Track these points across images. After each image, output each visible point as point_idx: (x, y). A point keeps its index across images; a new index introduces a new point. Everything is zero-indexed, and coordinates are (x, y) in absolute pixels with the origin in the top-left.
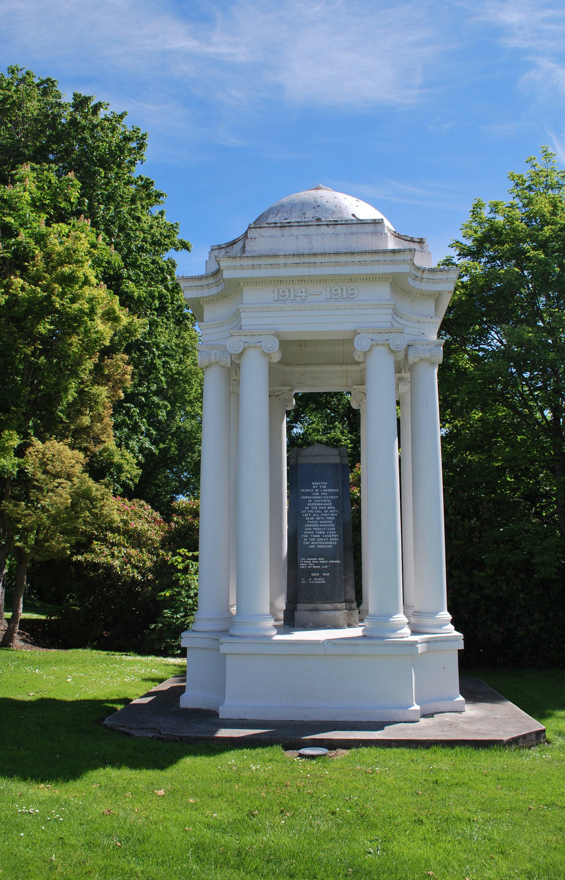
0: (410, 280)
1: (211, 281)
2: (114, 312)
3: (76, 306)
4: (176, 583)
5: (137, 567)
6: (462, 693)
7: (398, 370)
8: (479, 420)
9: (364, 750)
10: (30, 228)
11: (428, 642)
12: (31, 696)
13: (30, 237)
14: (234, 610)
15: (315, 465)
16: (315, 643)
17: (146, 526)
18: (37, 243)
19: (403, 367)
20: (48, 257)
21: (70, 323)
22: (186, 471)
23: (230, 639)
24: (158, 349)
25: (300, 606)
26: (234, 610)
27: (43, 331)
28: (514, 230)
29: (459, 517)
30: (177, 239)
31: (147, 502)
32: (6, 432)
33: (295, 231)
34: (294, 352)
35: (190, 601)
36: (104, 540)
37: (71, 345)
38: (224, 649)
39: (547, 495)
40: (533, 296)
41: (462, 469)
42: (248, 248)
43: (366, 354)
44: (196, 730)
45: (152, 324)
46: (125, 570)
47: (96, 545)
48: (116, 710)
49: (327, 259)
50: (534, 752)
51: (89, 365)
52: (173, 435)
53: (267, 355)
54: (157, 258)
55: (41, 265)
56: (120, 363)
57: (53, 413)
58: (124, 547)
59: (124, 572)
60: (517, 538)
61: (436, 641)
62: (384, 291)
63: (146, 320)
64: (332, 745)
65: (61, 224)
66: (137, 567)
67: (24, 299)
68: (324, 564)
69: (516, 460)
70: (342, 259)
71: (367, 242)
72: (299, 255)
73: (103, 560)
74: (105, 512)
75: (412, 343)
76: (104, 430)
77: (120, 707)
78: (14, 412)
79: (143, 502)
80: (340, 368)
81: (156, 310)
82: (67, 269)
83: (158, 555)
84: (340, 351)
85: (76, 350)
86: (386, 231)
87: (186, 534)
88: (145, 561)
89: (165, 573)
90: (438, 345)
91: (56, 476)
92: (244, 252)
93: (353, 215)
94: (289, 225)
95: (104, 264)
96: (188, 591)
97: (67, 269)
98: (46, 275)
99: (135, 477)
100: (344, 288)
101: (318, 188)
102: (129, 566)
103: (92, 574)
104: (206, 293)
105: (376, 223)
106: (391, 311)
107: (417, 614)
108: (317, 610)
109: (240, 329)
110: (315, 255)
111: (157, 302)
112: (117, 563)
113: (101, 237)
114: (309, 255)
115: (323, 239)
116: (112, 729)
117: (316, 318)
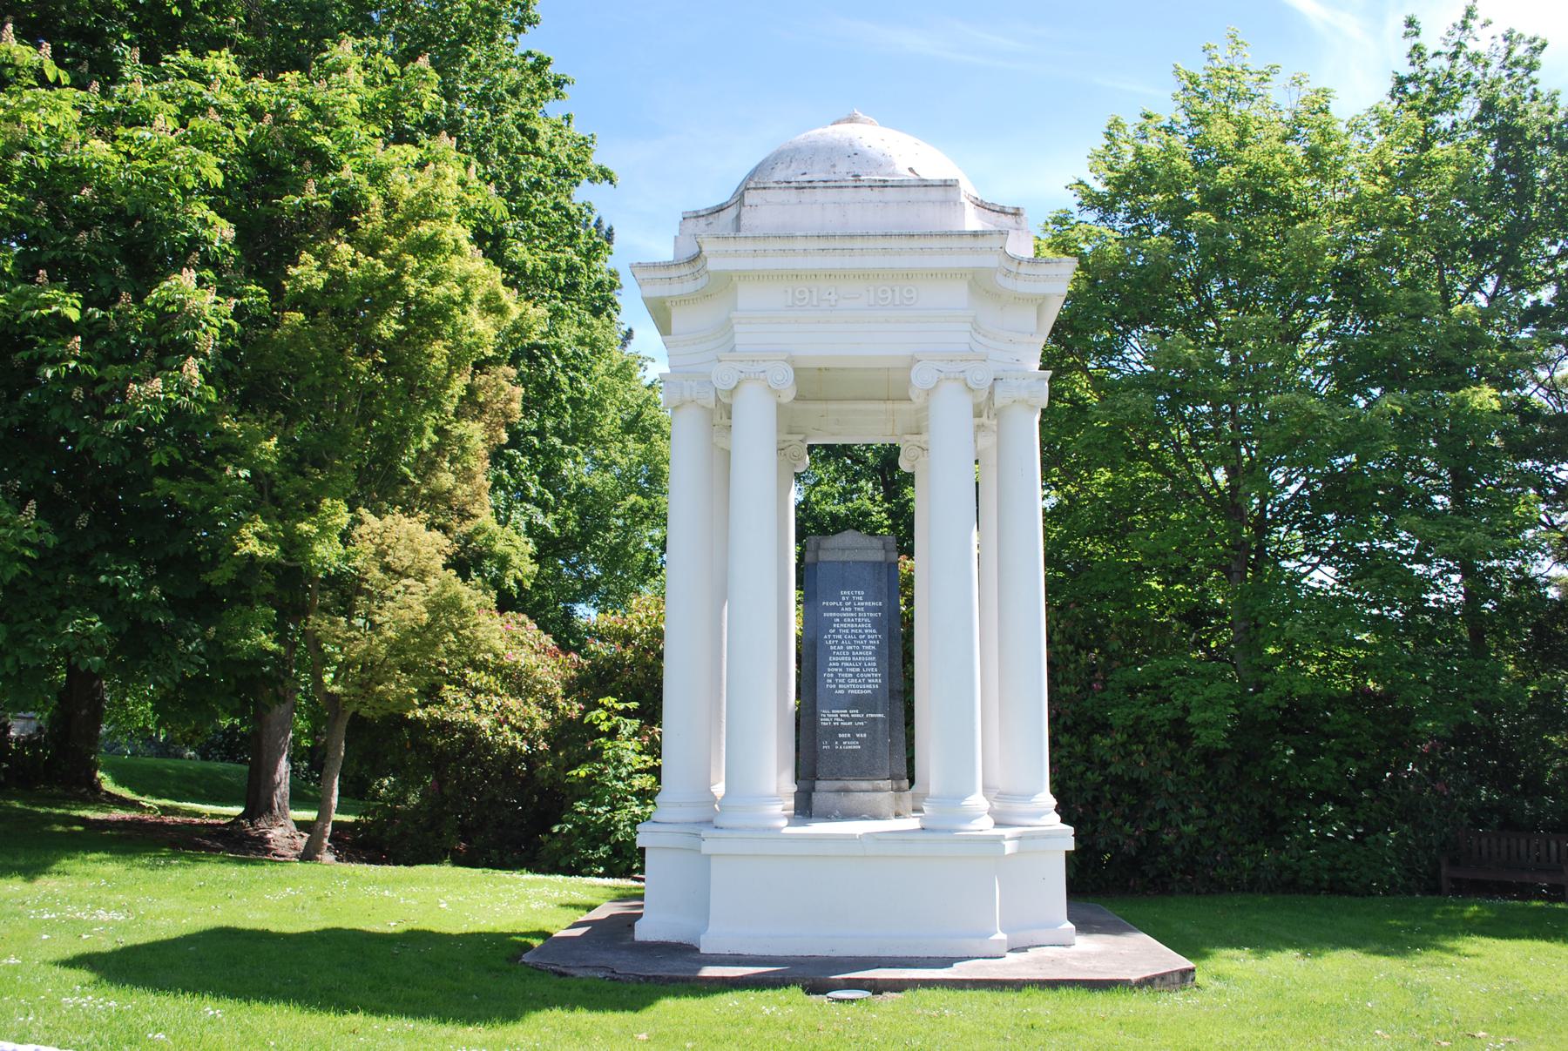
0: (1000, 278)
1: (686, 270)
2: (498, 298)
3: (439, 291)
4: (596, 754)
5: (520, 730)
6: (1069, 919)
7: (978, 414)
8: (1107, 485)
9: (923, 992)
10: (358, 156)
11: (1019, 838)
12: (393, 926)
13: (361, 172)
14: (719, 789)
15: (844, 563)
16: (850, 839)
17: (533, 659)
18: (373, 181)
19: (985, 410)
20: (390, 204)
21: (428, 319)
22: (593, 561)
23: (717, 833)
24: (559, 354)
25: (820, 785)
26: (719, 789)
27: (387, 334)
28: (1171, 173)
29: (1070, 648)
30: (593, 162)
31: (531, 618)
32: (327, 501)
33: (819, 194)
34: (815, 385)
35: (620, 785)
36: (461, 683)
37: (431, 356)
38: (706, 847)
39: (1220, 613)
40: (1199, 283)
41: (1077, 565)
42: (744, 221)
43: (928, 393)
44: (665, 968)
45: (557, 314)
46: (500, 734)
47: (448, 691)
48: (531, 947)
49: (871, 244)
50: (1178, 997)
51: (458, 386)
52: (571, 498)
53: (777, 394)
54: (562, 200)
55: (380, 222)
56: (504, 383)
57: (393, 468)
58: (497, 694)
59: (499, 739)
60: (1164, 683)
61: (1033, 837)
62: (957, 294)
63: (542, 311)
64: (877, 987)
65: (406, 146)
66: (520, 730)
67: (356, 281)
68: (858, 720)
69: (1165, 555)
70: (894, 243)
71: (931, 216)
72: (827, 237)
73: (461, 717)
74: (480, 635)
75: (1001, 375)
76: (476, 495)
77: (537, 943)
78: (339, 469)
79: (523, 617)
80: (882, 406)
81: (560, 290)
82: (425, 229)
83: (555, 710)
84: (890, 387)
85: (438, 364)
86: (963, 199)
87: (608, 673)
88: (531, 719)
89: (574, 739)
90: (1041, 379)
91: (402, 574)
92: (738, 229)
93: (911, 170)
94: (810, 185)
95: (478, 215)
96: (616, 768)
97: (425, 229)
98: (391, 239)
99: (528, 577)
100: (897, 289)
101: (852, 119)
102: (506, 727)
103: (440, 742)
104: (676, 289)
105: (947, 185)
106: (968, 327)
107: (1003, 796)
108: (847, 791)
109: (733, 350)
110: (852, 236)
111: (562, 276)
112: (485, 722)
113: (473, 169)
114: (843, 236)
115: (862, 212)
116: (536, 968)
117: (853, 336)
